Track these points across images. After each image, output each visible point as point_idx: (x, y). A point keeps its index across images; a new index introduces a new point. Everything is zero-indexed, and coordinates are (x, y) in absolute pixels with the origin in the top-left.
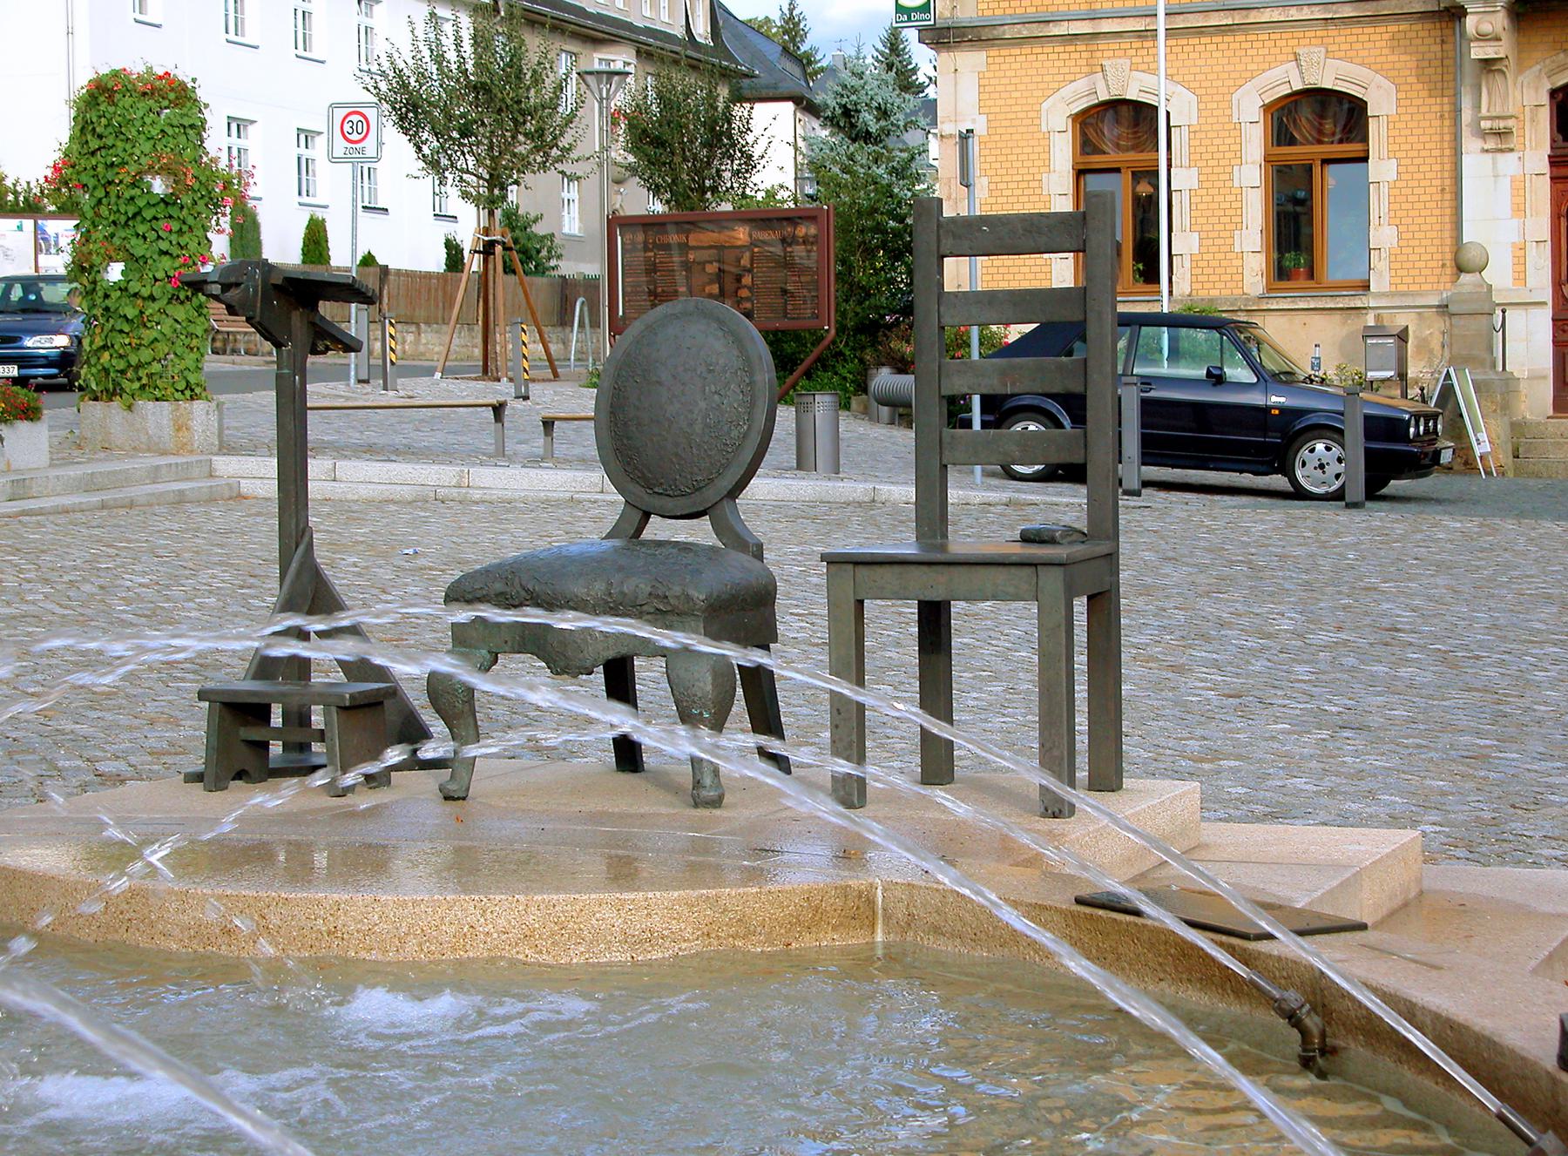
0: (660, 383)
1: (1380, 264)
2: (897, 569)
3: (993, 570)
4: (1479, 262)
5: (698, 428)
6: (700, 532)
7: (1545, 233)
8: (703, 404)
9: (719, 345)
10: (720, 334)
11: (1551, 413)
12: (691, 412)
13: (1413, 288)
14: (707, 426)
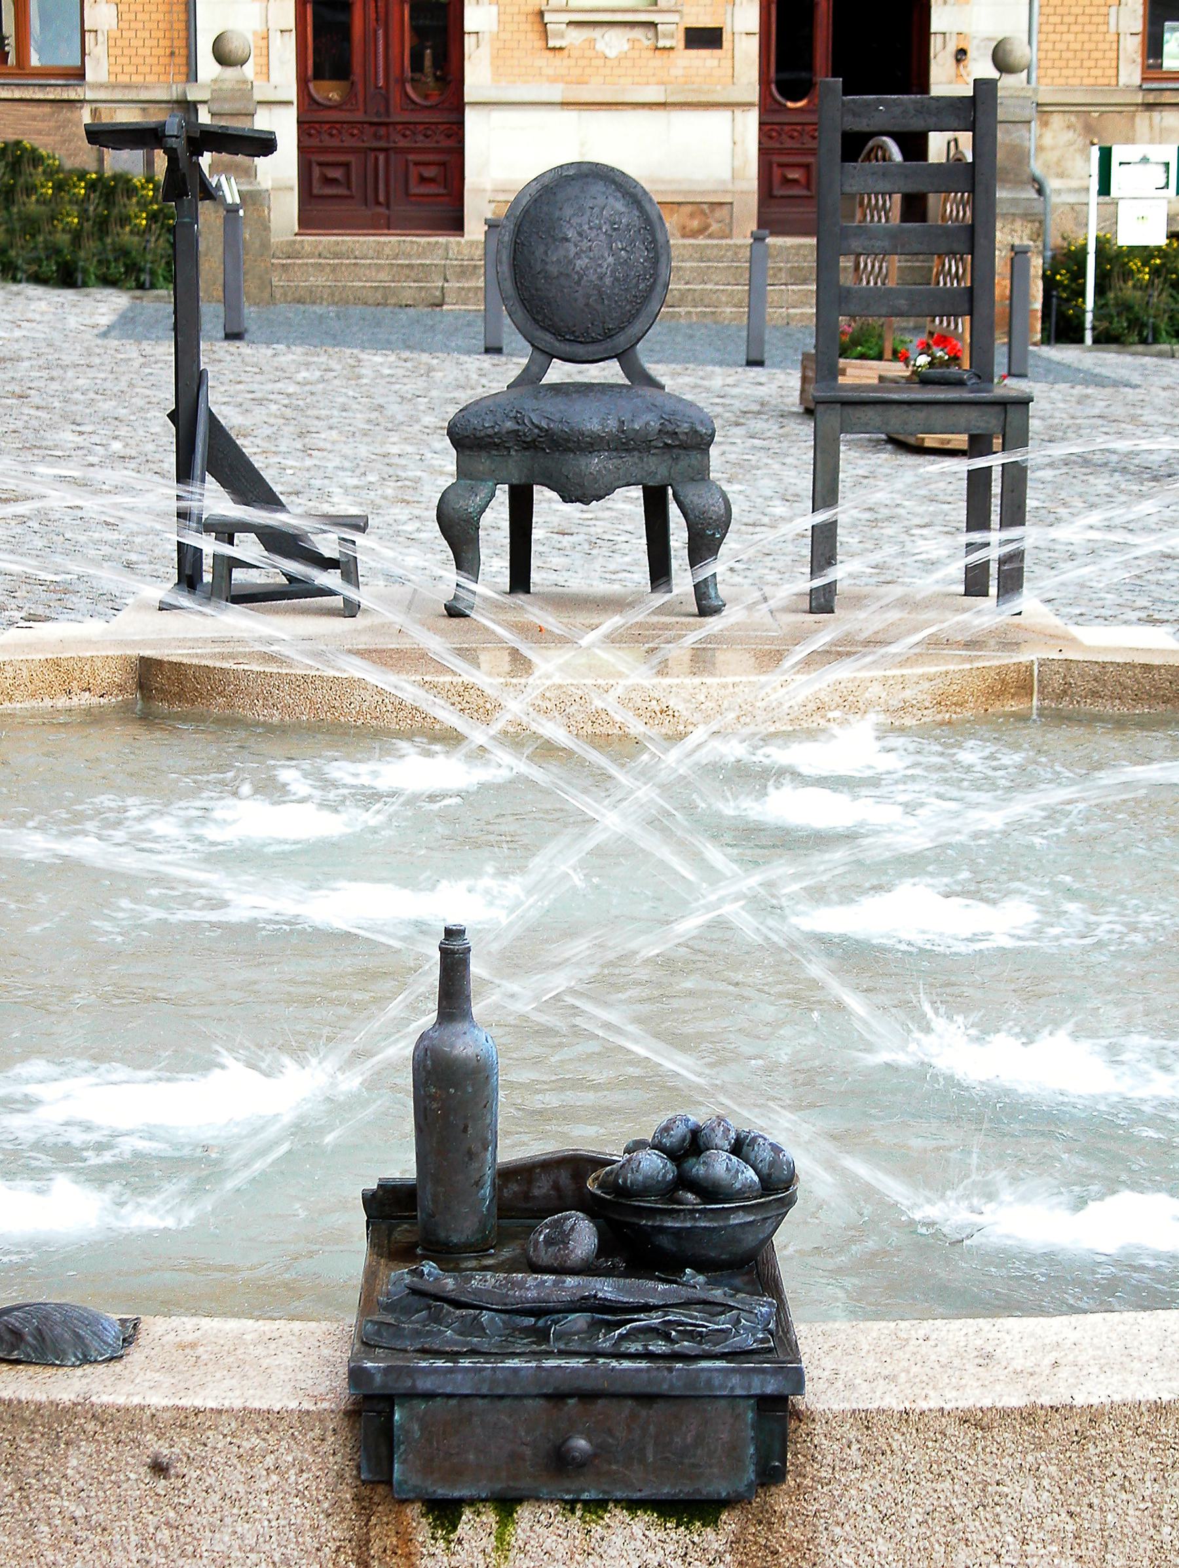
0: (567, 240)
1: (97, 51)
2: (879, 408)
3: (966, 409)
4: (245, 55)
5: (608, 281)
6: (609, 372)
7: (291, 23)
8: (611, 260)
9: (620, 206)
10: (619, 195)
11: (296, 229)
12: (600, 266)
13: (136, 79)
14: (617, 279)
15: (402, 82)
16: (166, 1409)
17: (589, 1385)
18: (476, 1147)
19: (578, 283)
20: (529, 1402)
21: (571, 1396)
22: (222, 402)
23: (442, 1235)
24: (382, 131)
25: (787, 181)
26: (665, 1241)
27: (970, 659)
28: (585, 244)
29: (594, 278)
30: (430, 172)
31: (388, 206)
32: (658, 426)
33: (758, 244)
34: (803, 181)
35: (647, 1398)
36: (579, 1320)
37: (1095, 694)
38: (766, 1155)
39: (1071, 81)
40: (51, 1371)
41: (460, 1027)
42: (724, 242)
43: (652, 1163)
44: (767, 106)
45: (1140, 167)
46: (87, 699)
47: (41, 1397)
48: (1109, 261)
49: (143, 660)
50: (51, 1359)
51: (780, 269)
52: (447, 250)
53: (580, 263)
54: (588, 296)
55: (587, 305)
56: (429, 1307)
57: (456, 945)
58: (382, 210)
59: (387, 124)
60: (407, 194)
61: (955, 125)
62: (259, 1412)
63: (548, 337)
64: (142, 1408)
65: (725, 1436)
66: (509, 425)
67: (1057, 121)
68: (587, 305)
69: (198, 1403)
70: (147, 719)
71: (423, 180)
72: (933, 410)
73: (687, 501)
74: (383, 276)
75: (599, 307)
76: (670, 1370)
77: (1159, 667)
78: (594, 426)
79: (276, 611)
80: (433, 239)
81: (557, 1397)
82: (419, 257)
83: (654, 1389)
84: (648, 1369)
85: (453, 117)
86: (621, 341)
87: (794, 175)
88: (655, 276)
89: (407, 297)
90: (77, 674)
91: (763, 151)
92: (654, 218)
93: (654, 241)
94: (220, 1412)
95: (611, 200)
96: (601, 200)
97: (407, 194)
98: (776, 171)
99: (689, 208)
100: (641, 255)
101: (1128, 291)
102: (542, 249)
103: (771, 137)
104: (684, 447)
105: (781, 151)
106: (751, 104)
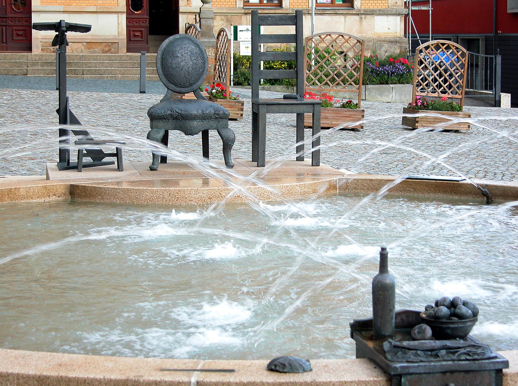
0: (178, 57)
2: (278, 106)
3: (303, 105)
5: (191, 69)
8: (191, 63)
9: (193, 47)
14: (193, 68)
15: (11, 4)
16: (337, 382)
17: (454, 368)
18: (392, 308)
19: (182, 70)
20: (437, 375)
21: (448, 372)
22: (73, 107)
23: (383, 333)
24: (4, 20)
25: (135, 36)
26: (449, 331)
27: (314, 179)
28: (183, 58)
29: (186, 68)
30: (20, 33)
31: (6, 44)
32: (213, 112)
33: (143, 55)
34: (140, 36)
35: (467, 372)
36: (443, 352)
37: (355, 188)
38: (472, 306)
39: (222, 6)
40: (297, 375)
41: (386, 275)
42: (117, 54)
43: (444, 310)
44: (128, 13)
45: (246, 32)
46: (54, 198)
47: (301, 381)
48: (237, 60)
49: (72, 186)
50: (295, 371)
51: (135, 63)
52: (27, 57)
53: (182, 64)
54: (185, 74)
55: (185, 76)
56: (401, 351)
57: (385, 252)
58: (5, 45)
59: (6, 18)
60: (13, 40)
61: (291, 23)
62: (362, 381)
63: (173, 86)
64: (330, 382)
65: (487, 381)
66: (169, 112)
67: (218, 18)
68: (185, 76)
69: (346, 380)
70: (72, 203)
71: (18, 35)
72: (293, 106)
73: (223, 134)
74: (6, 66)
75: (188, 77)
76: (475, 363)
77: (374, 180)
78: (195, 112)
79: (94, 170)
80: (23, 54)
81: (444, 373)
82: (18, 59)
83: (470, 369)
84: (469, 364)
85: (28, 16)
86: (195, 87)
87: (137, 34)
88: (204, 67)
89: (15, 72)
90: (51, 190)
91: (127, 27)
92: (204, 50)
93: (204, 57)
94: (352, 382)
95: (191, 45)
96: (188, 45)
97: (13, 40)
98: (132, 33)
99: (104, 44)
100: (200, 61)
101: (243, 69)
102: (171, 59)
103: (130, 22)
104: (221, 118)
105: (133, 27)
106: (124, 12)
